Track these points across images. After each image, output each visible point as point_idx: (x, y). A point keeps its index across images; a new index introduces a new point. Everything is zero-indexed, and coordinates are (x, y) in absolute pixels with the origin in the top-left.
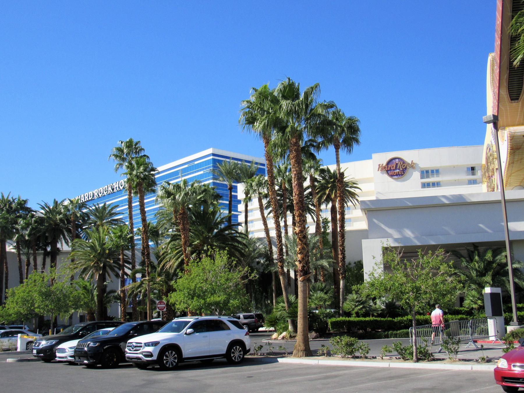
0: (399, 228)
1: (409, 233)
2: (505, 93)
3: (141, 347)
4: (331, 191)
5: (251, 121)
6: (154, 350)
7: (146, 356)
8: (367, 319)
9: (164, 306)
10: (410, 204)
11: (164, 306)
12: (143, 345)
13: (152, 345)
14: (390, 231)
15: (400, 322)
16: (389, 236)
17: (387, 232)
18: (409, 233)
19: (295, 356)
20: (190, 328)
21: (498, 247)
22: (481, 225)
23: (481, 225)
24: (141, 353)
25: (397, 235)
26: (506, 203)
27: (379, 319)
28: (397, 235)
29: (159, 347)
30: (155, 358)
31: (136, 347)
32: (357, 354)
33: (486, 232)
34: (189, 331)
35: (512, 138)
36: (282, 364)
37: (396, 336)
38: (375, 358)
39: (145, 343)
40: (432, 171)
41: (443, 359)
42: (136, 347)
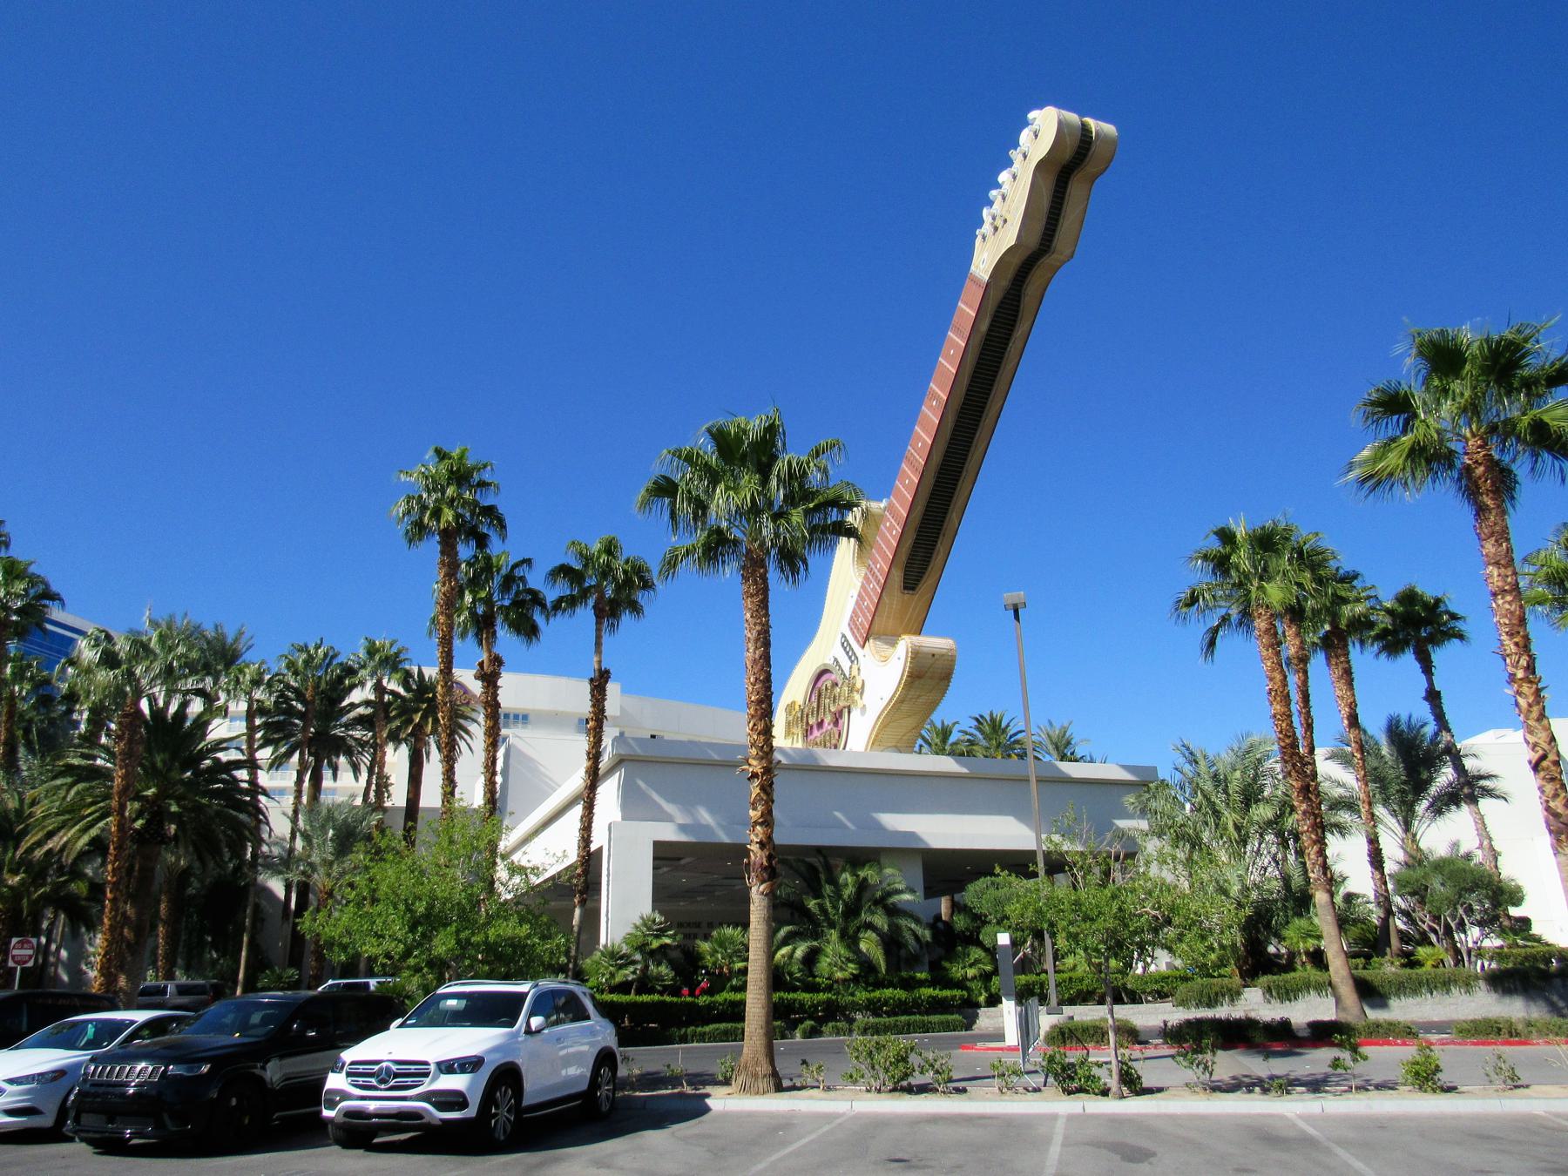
0: (687, 804)
1: (705, 817)
2: (898, 576)
3: (426, 1075)
4: (424, 718)
5: (419, 530)
6: (471, 1086)
7: (441, 1106)
8: (645, 998)
9: (30, 952)
10: (716, 757)
11: (30, 952)
12: (432, 1068)
13: (463, 1070)
14: (669, 808)
15: (710, 1007)
16: (668, 818)
17: (660, 807)
18: (705, 817)
19: (744, 1089)
20: (532, 1014)
21: (858, 857)
22: (837, 814)
23: (837, 814)
24: (425, 1097)
25: (681, 819)
26: (779, 781)
27: (668, 999)
28: (681, 819)
29: (485, 1073)
30: (471, 1112)
31: (396, 1075)
32: (917, 1079)
33: (846, 827)
34: (536, 1022)
35: (916, 655)
36: (726, 1116)
37: (702, 1038)
38: (964, 1091)
39: (439, 1064)
40: (516, 717)
41: (1160, 1090)
42: (396, 1075)
